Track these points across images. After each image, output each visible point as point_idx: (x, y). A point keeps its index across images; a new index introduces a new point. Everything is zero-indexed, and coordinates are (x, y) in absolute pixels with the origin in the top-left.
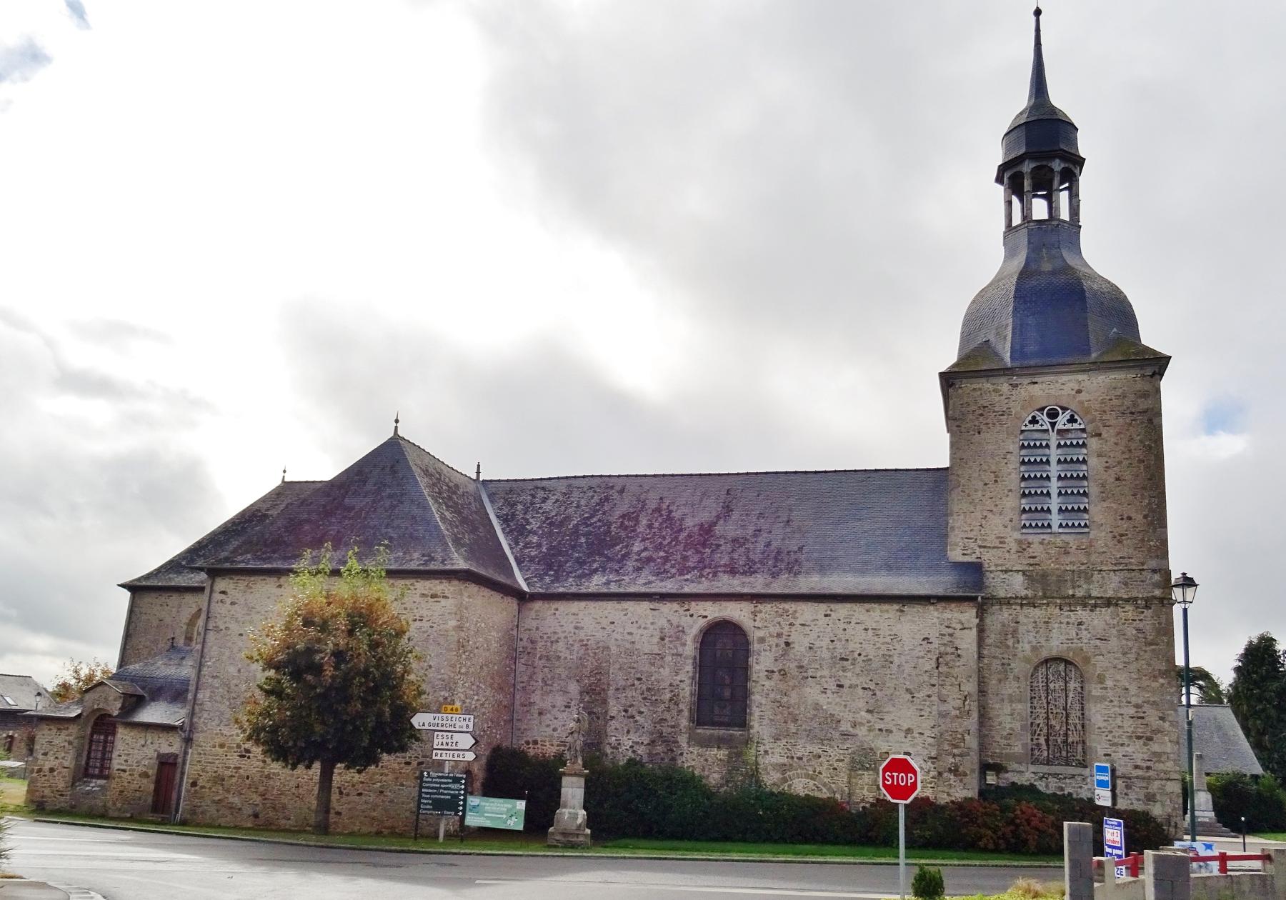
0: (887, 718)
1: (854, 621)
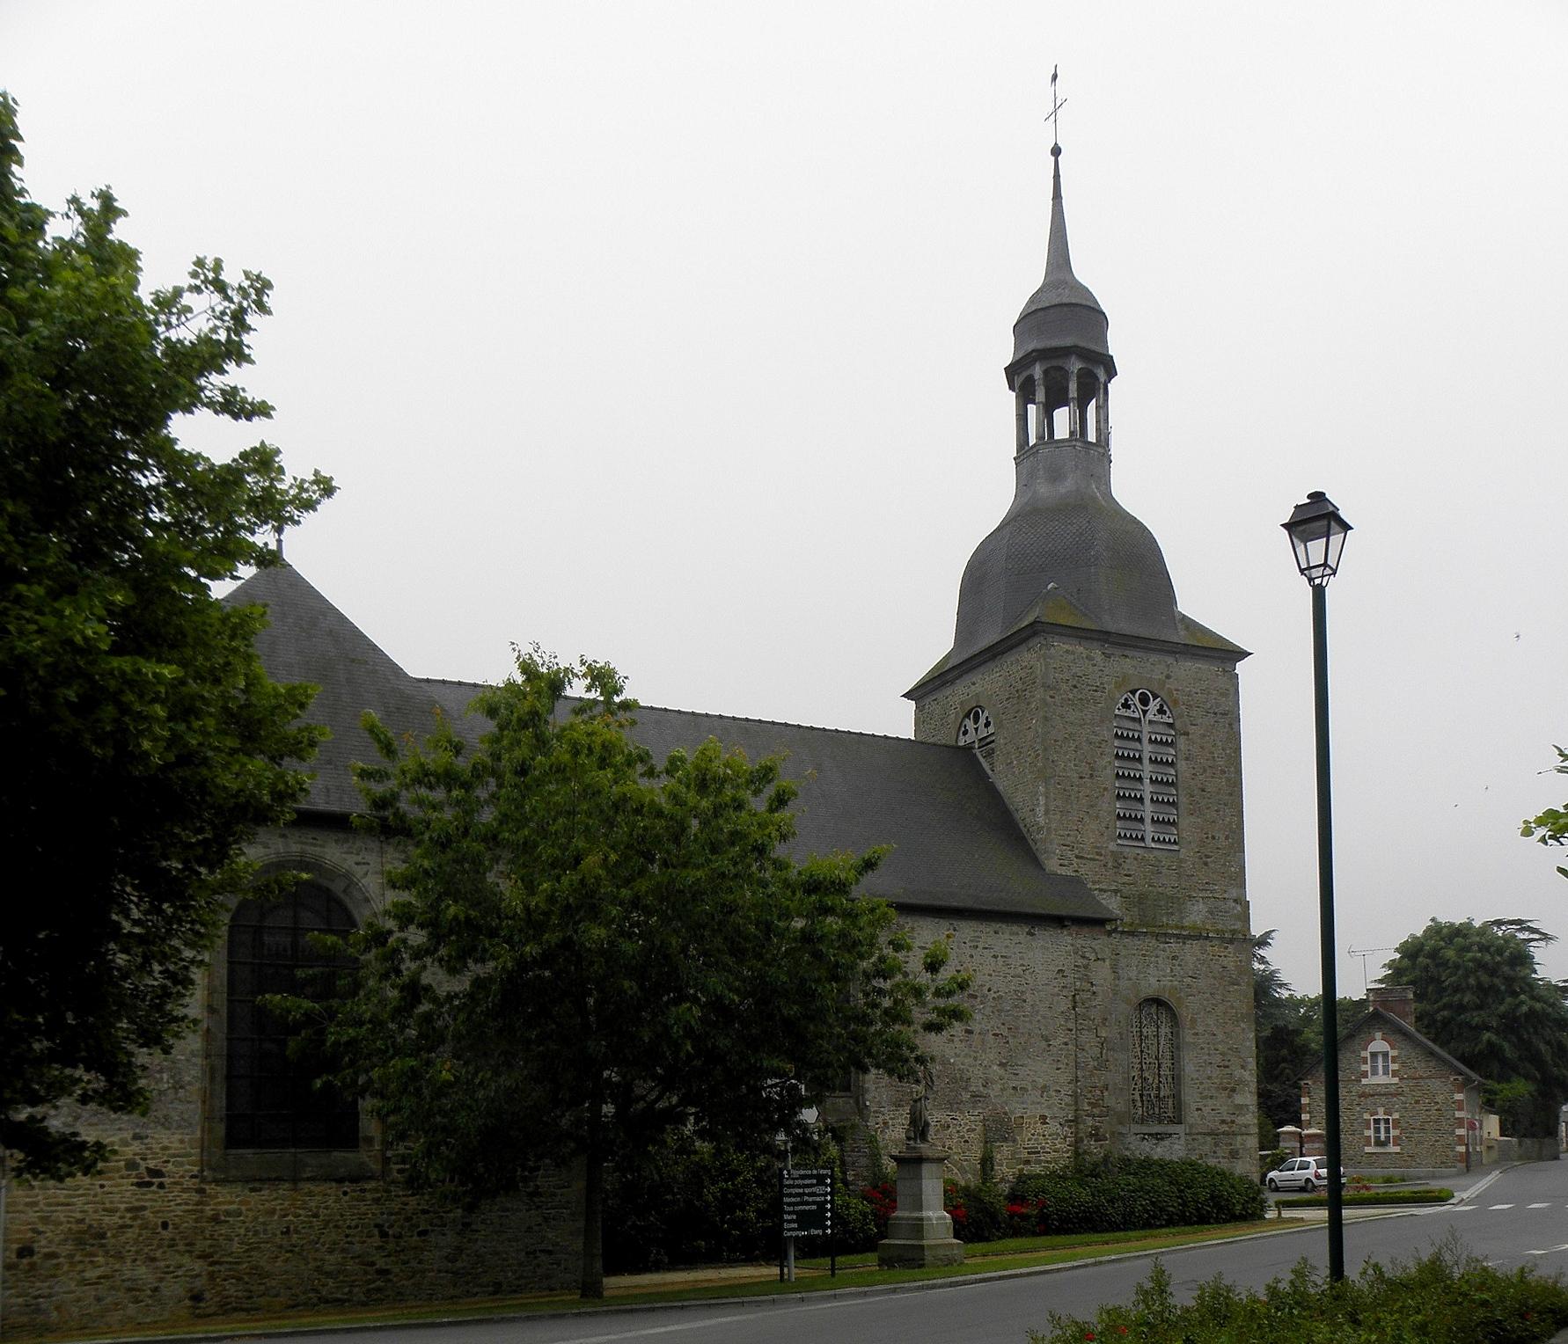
0: (1022, 1072)
1: (981, 945)
